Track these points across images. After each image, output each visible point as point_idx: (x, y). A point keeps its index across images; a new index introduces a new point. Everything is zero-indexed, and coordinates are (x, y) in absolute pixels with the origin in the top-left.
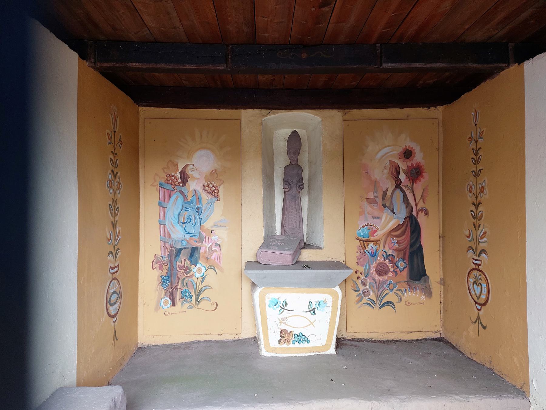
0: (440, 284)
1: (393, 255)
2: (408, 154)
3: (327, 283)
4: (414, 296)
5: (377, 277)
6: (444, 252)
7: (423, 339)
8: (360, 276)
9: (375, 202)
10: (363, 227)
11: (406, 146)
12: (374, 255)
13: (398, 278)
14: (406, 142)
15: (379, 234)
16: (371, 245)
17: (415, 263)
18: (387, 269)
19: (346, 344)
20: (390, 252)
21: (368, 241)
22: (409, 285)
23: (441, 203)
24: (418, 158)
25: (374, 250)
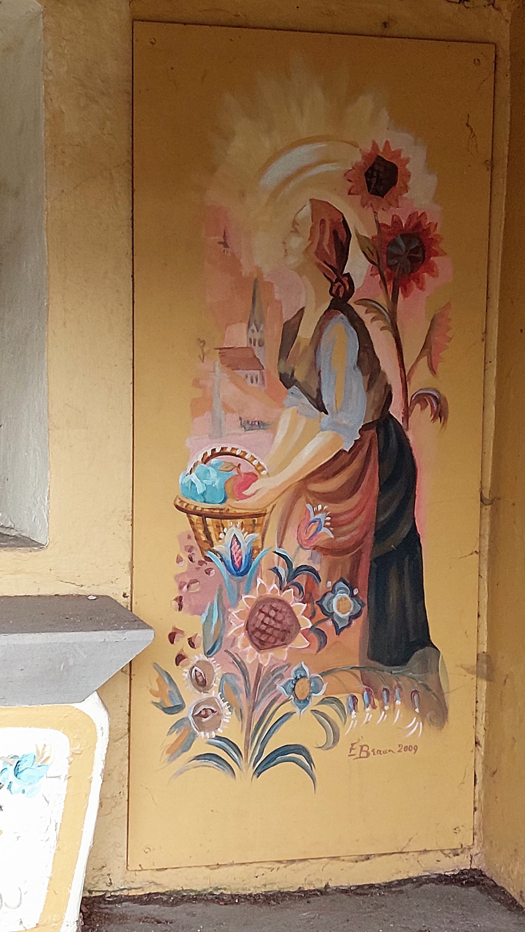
0: (479, 674)
1: (312, 570)
2: (380, 177)
3: (55, 685)
4: (385, 723)
5: (250, 655)
6: (495, 554)
7: (410, 880)
8: (188, 650)
9: (255, 363)
10: (206, 460)
11: (375, 146)
12: (241, 569)
13: (329, 657)
14: (374, 129)
15: (265, 491)
16: (232, 528)
17: (393, 598)
18: (288, 621)
19: (123, 917)
20: (302, 558)
21: (222, 516)
22: (367, 682)
23: (493, 372)
24: (419, 194)
25: (244, 551)
